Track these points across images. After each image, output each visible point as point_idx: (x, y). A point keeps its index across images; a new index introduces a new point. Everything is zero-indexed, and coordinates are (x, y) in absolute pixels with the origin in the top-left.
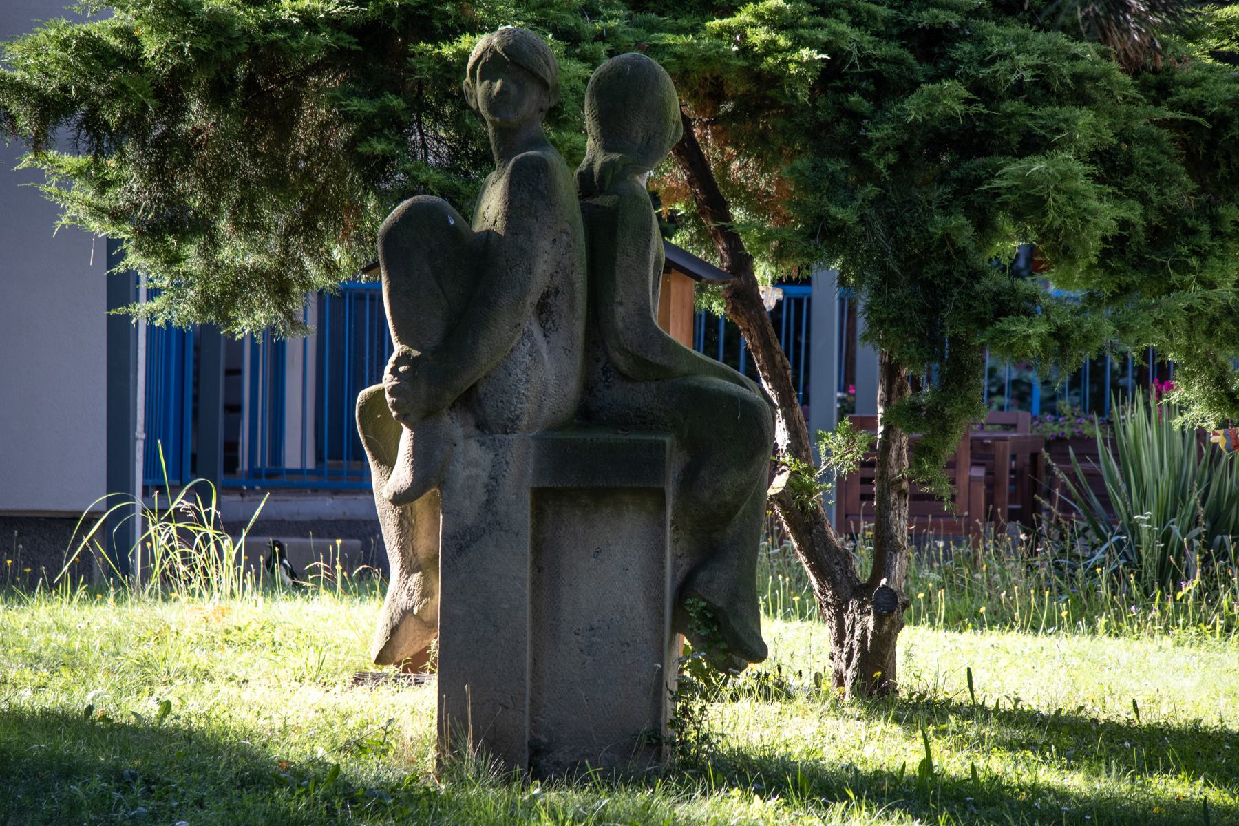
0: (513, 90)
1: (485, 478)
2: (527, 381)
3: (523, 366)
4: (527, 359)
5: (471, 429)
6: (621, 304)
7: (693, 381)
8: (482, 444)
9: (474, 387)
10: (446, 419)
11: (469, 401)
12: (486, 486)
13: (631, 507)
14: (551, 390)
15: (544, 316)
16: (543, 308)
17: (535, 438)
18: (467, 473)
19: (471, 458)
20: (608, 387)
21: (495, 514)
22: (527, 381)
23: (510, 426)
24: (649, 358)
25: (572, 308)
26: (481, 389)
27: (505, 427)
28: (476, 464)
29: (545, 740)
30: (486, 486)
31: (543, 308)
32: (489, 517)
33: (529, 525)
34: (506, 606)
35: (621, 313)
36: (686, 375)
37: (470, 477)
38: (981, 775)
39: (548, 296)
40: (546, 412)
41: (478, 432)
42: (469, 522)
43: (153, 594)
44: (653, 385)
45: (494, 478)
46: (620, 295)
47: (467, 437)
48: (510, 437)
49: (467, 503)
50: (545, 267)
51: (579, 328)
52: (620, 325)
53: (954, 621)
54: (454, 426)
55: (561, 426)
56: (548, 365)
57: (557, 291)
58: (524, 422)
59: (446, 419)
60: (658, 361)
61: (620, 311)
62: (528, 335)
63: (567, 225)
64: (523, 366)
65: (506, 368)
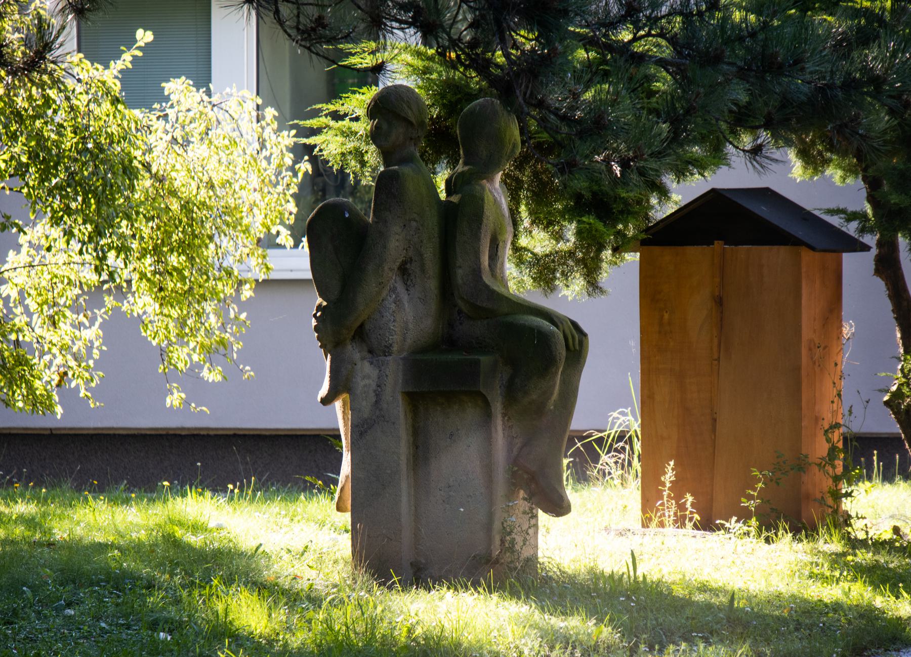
0: (385, 126)
1: (374, 386)
2: (394, 321)
3: (391, 311)
4: (393, 306)
5: (366, 354)
6: (460, 267)
7: (510, 319)
8: (371, 363)
9: (362, 326)
10: (349, 347)
11: (361, 334)
12: (375, 391)
13: (470, 405)
14: (411, 326)
15: (405, 277)
16: (403, 270)
17: (403, 359)
18: (362, 383)
19: (366, 373)
20: (461, 324)
21: (381, 410)
22: (394, 321)
23: (387, 351)
24: (478, 303)
25: (423, 270)
26: (367, 327)
27: (384, 352)
28: (369, 377)
29: (424, 561)
30: (375, 391)
31: (403, 270)
32: (378, 412)
33: (402, 416)
34: (389, 472)
35: (461, 274)
36: (507, 314)
37: (365, 386)
38: (648, 580)
39: (406, 263)
40: (409, 341)
41: (370, 356)
42: (366, 416)
43: (877, 481)
44: (485, 322)
45: (379, 386)
46: (459, 262)
47: (363, 359)
48: (388, 358)
49: (364, 403)
50: (397, 244)
51: (433, 285)
52: (460, 281)
53: (888, 478)
54: (353, 352)
55: (423, 350)
56: (408, 310)
57: (411, 260)
58: (395, 348)
59: (349, 347)
60: (484, 305)
61: (460, 272)
62: (393, 290)
63: (415, 215)
64: (391, 311)
65: (380, 312)
